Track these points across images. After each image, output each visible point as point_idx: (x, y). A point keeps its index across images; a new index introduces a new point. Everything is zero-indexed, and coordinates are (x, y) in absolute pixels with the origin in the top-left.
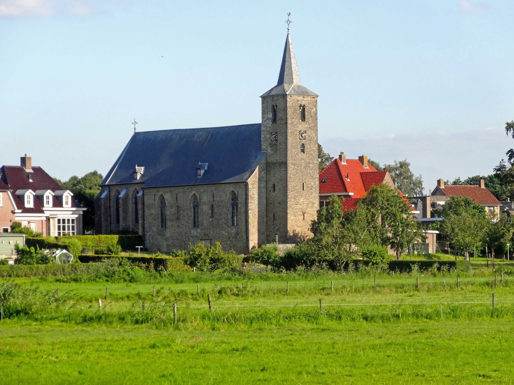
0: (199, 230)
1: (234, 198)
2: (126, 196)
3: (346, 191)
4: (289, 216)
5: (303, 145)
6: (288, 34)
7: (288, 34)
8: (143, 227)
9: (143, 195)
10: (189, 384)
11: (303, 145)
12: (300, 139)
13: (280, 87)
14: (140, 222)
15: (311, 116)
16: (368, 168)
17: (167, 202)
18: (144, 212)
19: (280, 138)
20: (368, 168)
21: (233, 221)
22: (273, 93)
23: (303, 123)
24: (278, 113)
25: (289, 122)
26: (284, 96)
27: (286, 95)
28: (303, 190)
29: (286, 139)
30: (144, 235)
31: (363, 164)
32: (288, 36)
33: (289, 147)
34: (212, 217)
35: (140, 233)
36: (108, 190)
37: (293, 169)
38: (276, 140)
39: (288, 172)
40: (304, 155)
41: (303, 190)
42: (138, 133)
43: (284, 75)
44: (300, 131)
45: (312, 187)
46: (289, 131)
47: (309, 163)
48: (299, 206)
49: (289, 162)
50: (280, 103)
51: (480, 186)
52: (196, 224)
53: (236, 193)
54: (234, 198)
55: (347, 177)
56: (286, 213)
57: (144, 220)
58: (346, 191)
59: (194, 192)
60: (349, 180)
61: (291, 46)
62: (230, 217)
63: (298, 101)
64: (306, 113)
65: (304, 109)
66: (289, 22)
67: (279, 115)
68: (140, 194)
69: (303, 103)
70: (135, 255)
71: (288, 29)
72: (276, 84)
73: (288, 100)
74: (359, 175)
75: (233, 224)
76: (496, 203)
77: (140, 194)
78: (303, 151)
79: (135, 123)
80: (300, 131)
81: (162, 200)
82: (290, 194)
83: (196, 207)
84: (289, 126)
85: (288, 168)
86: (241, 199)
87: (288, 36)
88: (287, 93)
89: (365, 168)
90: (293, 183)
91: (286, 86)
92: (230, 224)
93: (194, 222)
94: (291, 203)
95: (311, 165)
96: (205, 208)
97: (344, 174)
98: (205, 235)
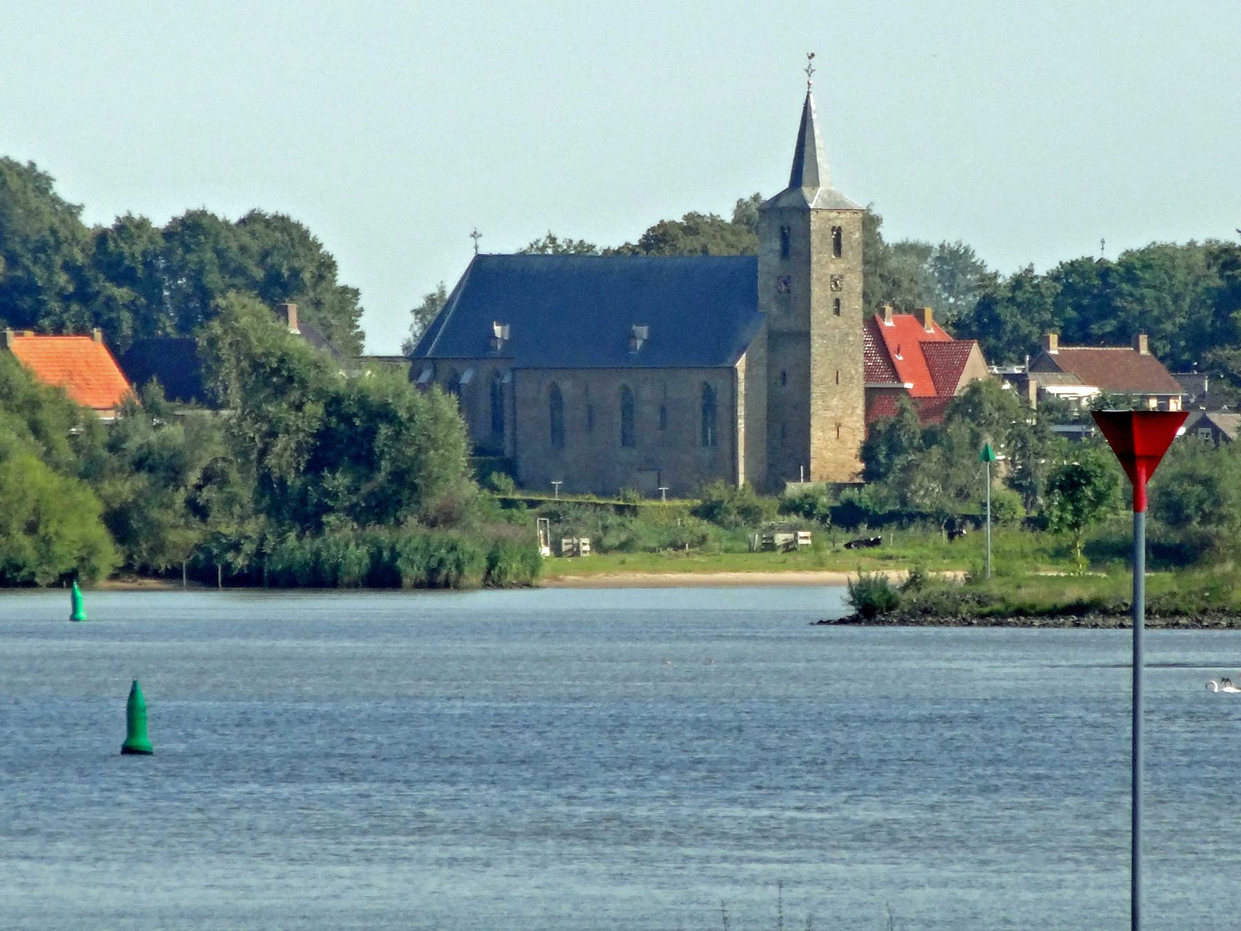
0: (635, 452)
1: (709, 396)
2: (475, 380)
3: (899, 381)
4: (813, 431)
5: (837, 302)
6: (809, 93)
7: (809, 93)
8: (515, 442)
9: (513, 381)
10: (11, 890)
11: (837, 302)
12: (832, 290)
13: (793, 195)
14: (508, 431)
15: (852, 248)
16: (932, 331)
17: (565, 400)
18: (515, 413)
19: (796, 286)
20: (932, 331)
21: (705, 437)
22: (783, 203)
23: (838, 261)
24: (791, 241)
25: (814, 258)
26: (805, 211)
27: (809, 210)
28: (837, 383)
29: (809, 290)
30: (516, 457)
31: (923, 323)
32: (808, 97)
33: (814, 304)
34: (663, 426)
35: (508, 455)
36: (432, 369)
37: (821, 346)
38: (789, 291)
39: (812, 350)
40: (839, 320)
41: (837, 383)
42: (483, 256)
43: (801, 171)
44: (832, 276)
45: (852, 378)
46: (814, 275)
47: (847, 334)
48: (829, 414)
49: (814, 332)
50: (795, 222)
51: (1137, 348)
52: (627, 440)
53: (713, 387)
54: (709, 396)
55: (898, 351)
56: (809, 425)
57: (515, 429)
58: (899, 381)
59: (622, 381)
60: (901, 358)
61: (814, 116)
62: (699, 427)
63: (829, 220)
64: (843, 242)
65: (838, 236)
66: (809, 71)
67: (795, 244)
68: (507, 379)
69: (838, 223)
70: (580, 499)
71: (809, 84)
72: (786, 186)
73: (812, 219)
74: (917, 344)
75: (705, 443)
76: (1175, 390)
77: (507, 379)
78: (837, 312)
79: (475, 235)
80: (832, 276)
81: (556, 396)
82: (816, 391)
83: (628, 407)
84: (813, 266)
85: (812, 343)
86: (722, 398)
87: (808, 97)
88: (812, 206)
89: (928, 332)
90: (820, 372)
91: (806, 191)
92: (699, 439)
93: (624, 435)
94: (816, 406)
95: (851, 339)
96: (647, 412)
97: (891, 344)
98: (648, 461)
